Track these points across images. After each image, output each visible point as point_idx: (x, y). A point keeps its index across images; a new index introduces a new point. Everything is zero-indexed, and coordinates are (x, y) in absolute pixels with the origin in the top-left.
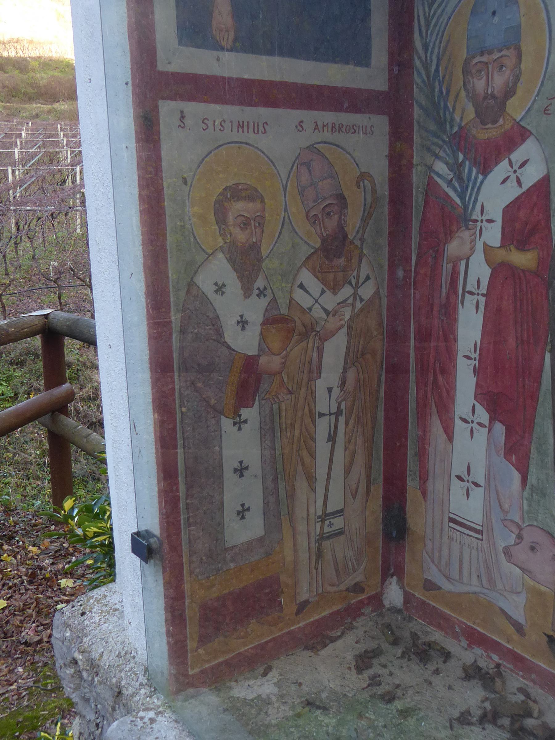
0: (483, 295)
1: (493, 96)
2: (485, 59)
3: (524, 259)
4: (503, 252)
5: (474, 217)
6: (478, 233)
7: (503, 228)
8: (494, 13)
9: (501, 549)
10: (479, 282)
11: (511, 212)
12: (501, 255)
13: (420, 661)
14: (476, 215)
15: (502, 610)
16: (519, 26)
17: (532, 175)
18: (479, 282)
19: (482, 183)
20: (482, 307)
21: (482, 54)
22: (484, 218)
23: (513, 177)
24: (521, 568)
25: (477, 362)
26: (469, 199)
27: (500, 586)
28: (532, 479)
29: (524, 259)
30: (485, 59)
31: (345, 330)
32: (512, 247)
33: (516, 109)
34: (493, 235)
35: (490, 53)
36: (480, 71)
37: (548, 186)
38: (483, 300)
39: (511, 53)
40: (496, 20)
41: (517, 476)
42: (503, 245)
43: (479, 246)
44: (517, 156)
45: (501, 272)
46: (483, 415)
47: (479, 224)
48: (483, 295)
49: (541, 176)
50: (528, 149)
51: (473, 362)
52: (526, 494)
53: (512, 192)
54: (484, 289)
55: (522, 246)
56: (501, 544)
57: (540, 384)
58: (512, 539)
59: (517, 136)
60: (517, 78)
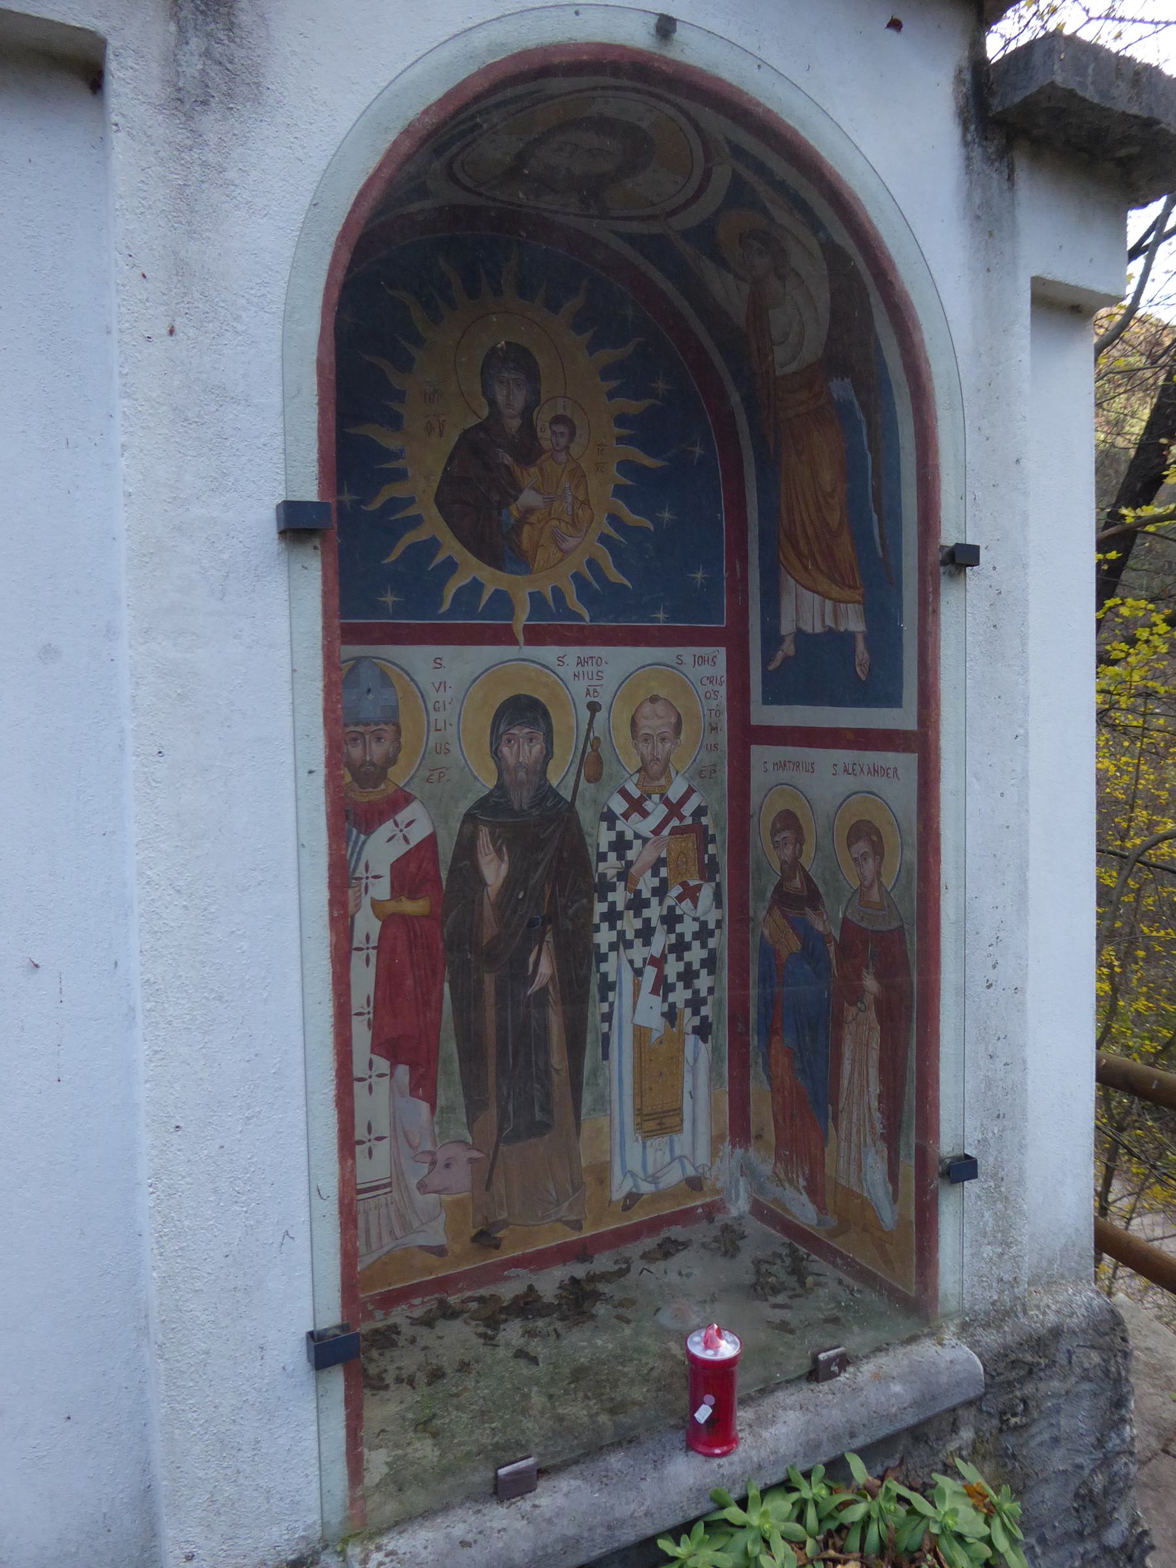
0: (374, 948)
1: (372, 764)
2: (360, 729)
3: (411, 907)
4: (393, 903)
5: (357, 875)
6: (363, 889)
7: (392, 883)
8: (369, 691)
9: (414, 1187)
10: (368, 938)
11: (398, 868)
12: (393, 907)
13: (573, 1278)
14: (360, 871)
15: (421, 1247)
16: (397, 706)
17: (418, 833)
18: (368, 938)
19: (364, 843)
20: (373, 960)
21: (357, 724)
22: (369, 875)
23: (400, 835)
24: (436, 1192)
25: (371, 1016)
26: (352, 855)
27: (416, 1224)
28: (441, 1101)
29: (411, 907)
30: (360, 729)
31: (800, 588)
32: (403, 898)
33: (398, 776)
34: (382, 890)
35: (367, 724)
36: (355, 740)
37: (435, 843)
38: (373, 954)
39: (390, 728)
40: (371, 697)
41: (424, 1107)
42: (393, 898)
43: (366, 902)
44: (403, 816)
45: (390, 921)
46: (382, 1064)
47: (364, 881)
48: (374, 948)
49: (428, 833)
50: (412, 811)
51: (366, 1017)
52: (435, 1119)
53: (399, 849)
54: (374, 942)
55: (412, 897)
56: (413, 1182)
57: (441, 1013)
58: (425, 1169)
59: (400, 800)
60: (399, 749)
